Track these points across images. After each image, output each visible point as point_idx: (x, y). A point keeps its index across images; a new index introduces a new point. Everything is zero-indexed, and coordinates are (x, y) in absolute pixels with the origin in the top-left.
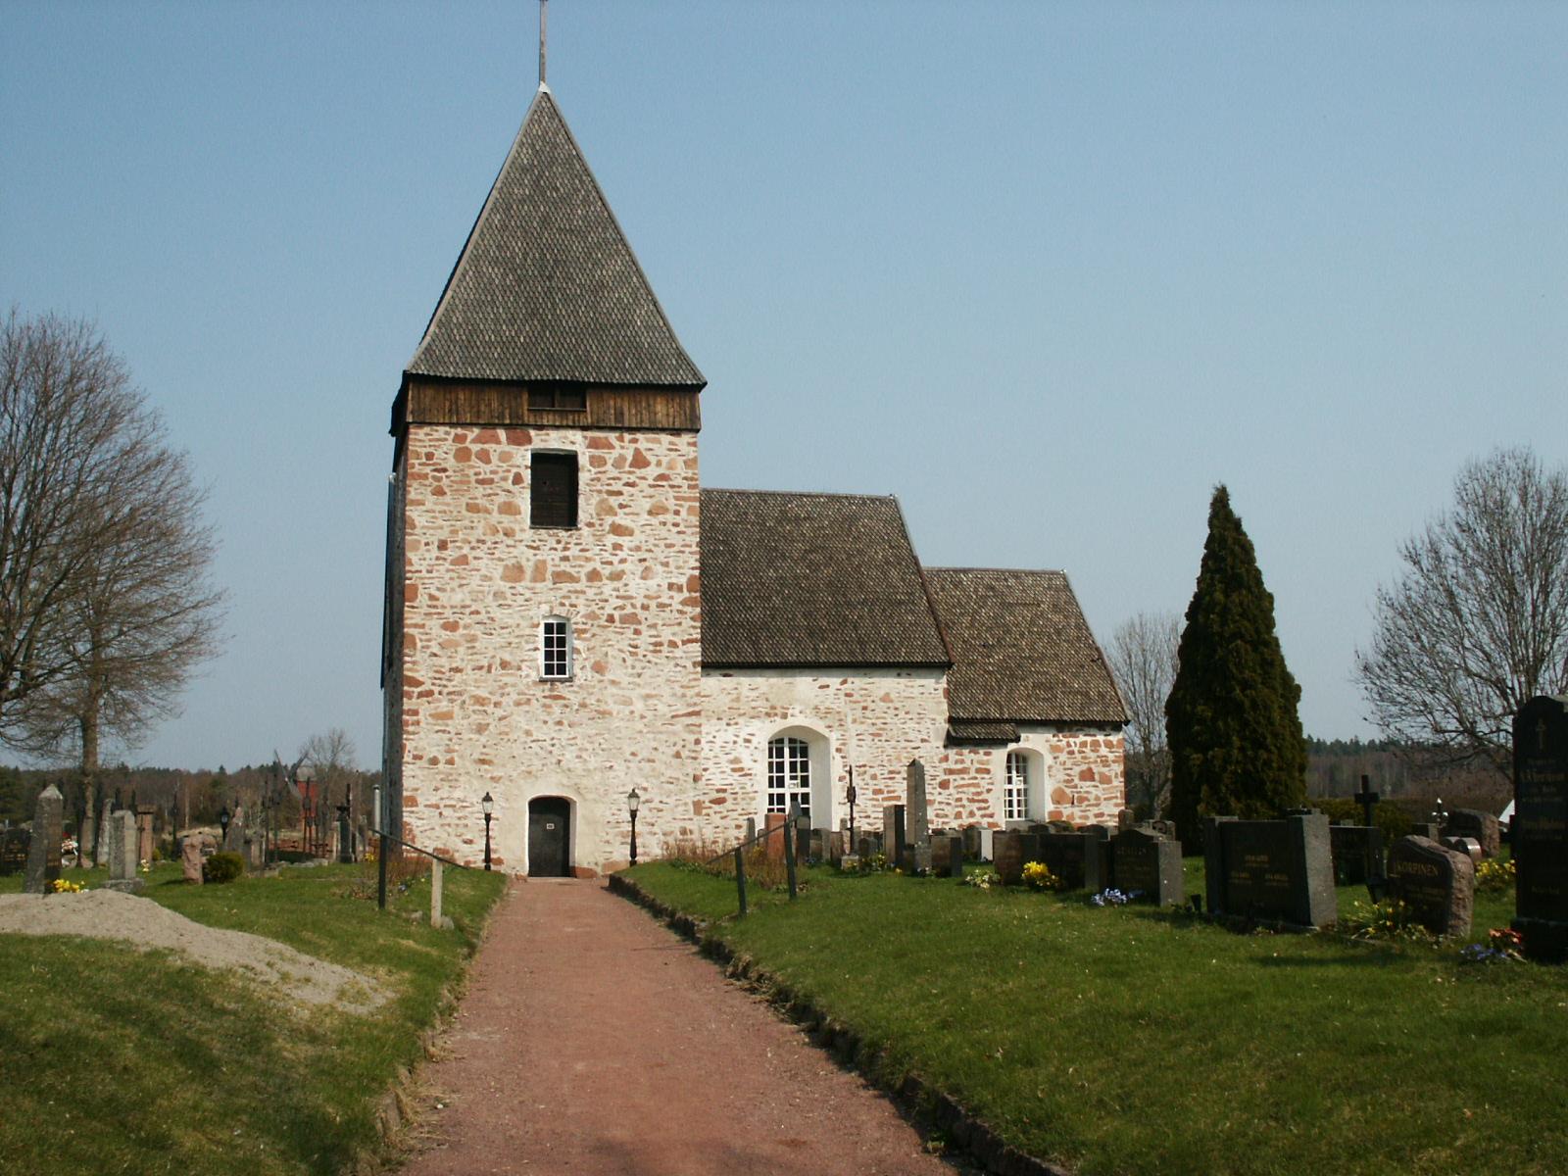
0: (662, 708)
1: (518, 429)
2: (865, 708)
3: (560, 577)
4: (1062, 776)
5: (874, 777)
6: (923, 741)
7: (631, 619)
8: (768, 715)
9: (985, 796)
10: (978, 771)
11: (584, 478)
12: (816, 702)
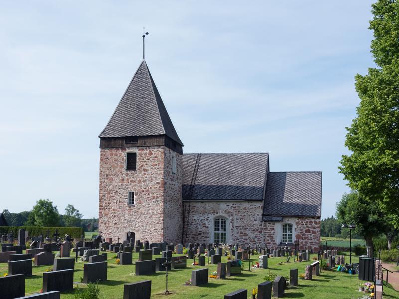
1: (123, 149)
2: (239, 211)
4: (299, 231)
5: (241, 229)
6: (255, 220)
8: (213, 213)
9: (272, 236)
10: (270, 229)
12: (226, 209)
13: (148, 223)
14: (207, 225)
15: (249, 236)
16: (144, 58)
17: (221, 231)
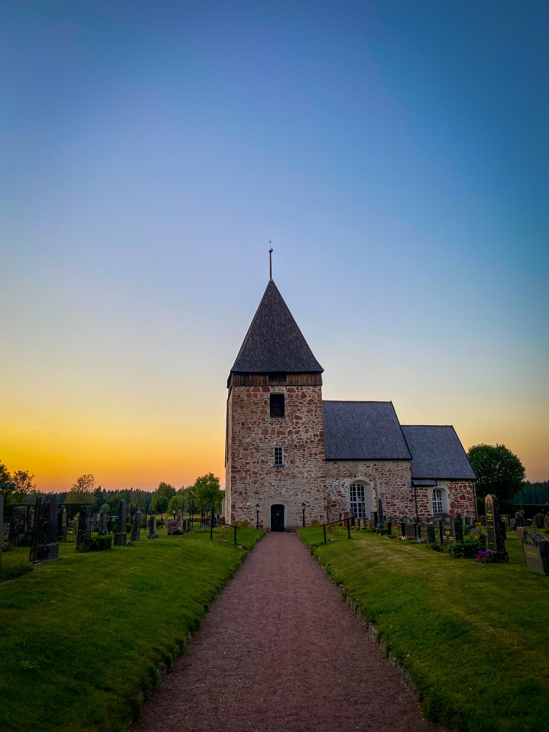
0: (313, 475)
2: (382, 474)
3: (279, 433)
5: (387, 498)
7: (302, 446)
8: (349, 476)
9: (426, 504)
10: (423, 496)
11: (286, 402)
12: (366, 472)
13: (304, 490)
14: (343, 492)
15: (397, 506)
16: (271, 277)
17: (358, 501)
